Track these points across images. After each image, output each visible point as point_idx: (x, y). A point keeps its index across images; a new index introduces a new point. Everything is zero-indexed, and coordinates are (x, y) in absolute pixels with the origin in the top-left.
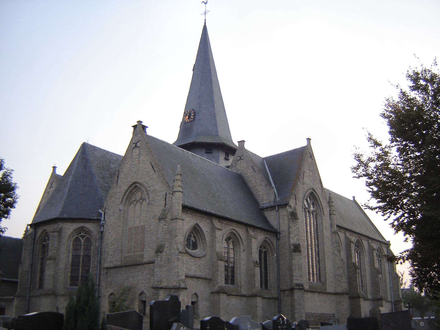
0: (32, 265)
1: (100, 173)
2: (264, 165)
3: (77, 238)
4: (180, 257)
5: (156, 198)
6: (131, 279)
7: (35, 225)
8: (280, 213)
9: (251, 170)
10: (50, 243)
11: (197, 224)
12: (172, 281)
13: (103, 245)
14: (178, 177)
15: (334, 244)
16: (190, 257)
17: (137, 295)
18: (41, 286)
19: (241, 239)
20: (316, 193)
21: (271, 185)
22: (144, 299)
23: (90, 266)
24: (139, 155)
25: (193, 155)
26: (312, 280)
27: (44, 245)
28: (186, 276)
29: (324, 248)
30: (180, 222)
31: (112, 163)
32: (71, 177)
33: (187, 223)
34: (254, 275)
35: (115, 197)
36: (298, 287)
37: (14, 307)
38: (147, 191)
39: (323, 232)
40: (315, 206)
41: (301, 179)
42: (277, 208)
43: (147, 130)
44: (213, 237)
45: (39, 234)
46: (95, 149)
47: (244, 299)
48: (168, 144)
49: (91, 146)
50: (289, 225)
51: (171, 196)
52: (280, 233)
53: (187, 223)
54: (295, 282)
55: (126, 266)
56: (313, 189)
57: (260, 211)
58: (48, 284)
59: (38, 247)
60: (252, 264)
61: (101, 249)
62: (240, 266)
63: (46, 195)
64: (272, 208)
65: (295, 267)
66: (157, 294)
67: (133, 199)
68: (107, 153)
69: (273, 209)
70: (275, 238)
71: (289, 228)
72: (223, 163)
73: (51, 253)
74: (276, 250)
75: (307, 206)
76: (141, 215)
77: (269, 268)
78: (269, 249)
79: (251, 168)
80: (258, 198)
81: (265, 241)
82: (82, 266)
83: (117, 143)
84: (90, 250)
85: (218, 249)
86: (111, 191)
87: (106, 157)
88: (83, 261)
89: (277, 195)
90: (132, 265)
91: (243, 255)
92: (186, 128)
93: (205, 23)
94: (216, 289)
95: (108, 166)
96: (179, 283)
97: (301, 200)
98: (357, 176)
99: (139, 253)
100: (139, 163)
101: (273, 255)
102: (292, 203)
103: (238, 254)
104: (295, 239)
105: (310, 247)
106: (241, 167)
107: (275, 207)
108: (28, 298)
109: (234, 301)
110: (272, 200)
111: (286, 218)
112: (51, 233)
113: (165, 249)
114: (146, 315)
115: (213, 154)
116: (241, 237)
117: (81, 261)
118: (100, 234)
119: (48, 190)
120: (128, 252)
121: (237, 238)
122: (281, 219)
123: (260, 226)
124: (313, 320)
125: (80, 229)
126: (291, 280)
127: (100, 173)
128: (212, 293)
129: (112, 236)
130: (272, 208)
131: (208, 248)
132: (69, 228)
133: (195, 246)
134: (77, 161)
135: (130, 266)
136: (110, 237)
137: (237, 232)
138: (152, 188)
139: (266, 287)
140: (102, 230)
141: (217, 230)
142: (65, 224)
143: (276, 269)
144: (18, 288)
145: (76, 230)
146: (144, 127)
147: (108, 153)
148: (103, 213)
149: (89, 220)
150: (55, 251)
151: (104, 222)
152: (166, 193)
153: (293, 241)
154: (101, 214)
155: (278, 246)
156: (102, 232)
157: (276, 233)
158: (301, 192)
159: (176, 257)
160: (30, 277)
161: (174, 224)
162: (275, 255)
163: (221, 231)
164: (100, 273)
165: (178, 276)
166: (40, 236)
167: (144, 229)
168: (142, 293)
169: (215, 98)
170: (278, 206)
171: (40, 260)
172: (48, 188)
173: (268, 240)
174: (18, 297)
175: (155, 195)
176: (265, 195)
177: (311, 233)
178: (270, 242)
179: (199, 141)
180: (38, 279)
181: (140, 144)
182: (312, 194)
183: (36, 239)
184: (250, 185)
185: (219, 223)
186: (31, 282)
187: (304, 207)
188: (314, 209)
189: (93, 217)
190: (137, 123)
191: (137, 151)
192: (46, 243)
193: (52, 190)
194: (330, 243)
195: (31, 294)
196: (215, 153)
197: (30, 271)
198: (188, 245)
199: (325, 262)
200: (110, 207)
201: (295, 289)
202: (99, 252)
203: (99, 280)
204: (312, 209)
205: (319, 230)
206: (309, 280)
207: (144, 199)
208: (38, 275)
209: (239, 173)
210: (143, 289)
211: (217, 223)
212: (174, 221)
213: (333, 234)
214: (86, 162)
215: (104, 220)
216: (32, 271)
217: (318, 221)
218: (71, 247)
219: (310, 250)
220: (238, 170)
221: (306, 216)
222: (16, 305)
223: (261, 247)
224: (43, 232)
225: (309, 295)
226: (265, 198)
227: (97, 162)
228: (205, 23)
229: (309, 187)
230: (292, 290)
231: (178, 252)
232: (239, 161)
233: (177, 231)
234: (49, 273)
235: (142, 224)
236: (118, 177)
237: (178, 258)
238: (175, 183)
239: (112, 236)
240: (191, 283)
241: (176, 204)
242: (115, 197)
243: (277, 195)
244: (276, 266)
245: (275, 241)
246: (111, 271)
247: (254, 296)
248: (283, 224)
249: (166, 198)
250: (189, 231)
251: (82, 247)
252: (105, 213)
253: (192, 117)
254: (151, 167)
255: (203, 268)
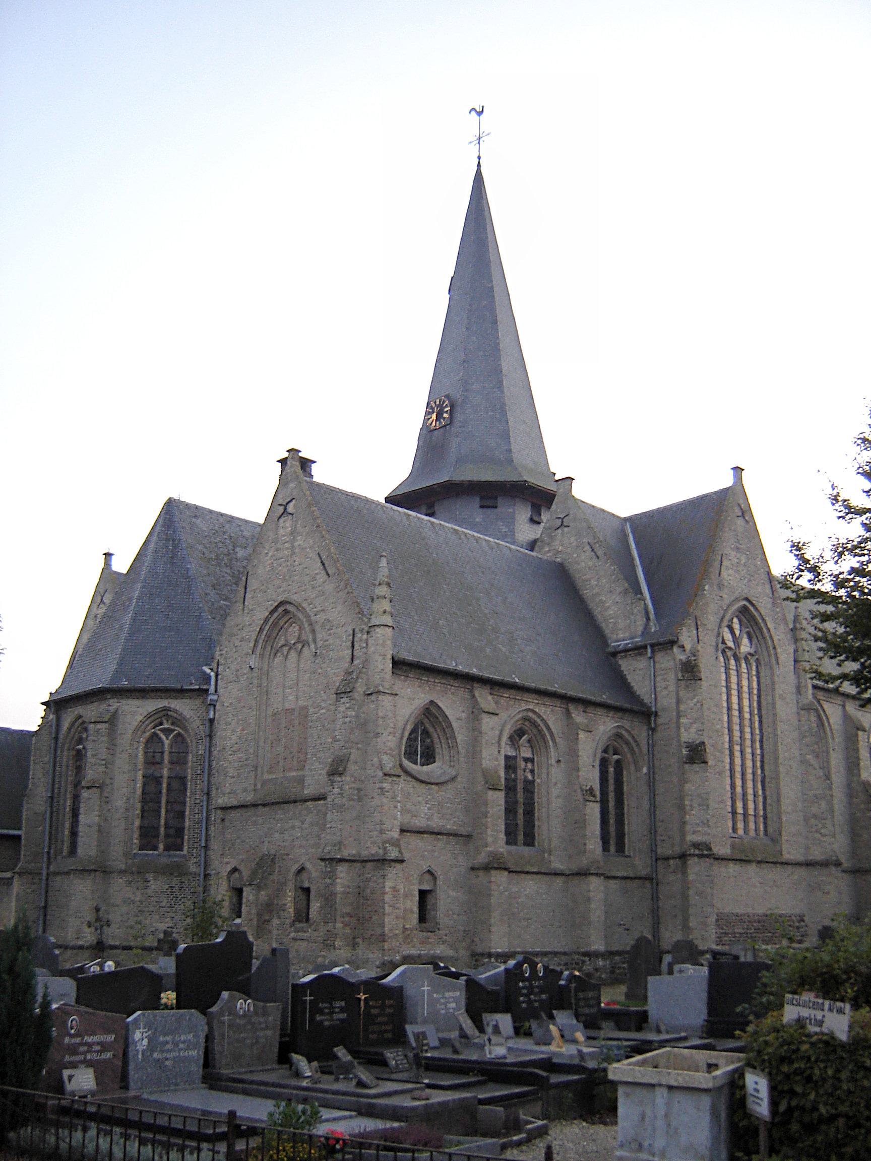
0: (52, 798)
1: (209, 574)
2: (625, 536)
3: (154, 734)
4: (385, 785)
5: (331, 641)
6: (277, 835)
7: (56, 705)
8: (657, 665)
9: (589, 553)
10: (90, 748)
11: (432, 702)
12: (369, 844)
13: (215, 753)
14: (383, 590)
15: (805, 737)
16: (414, 783)
17: (291, 875)
18: (73, 850)
19: (552, 735)
20: (756, 609)
21: (639, 591)
22: (306, 885)
23: (184, 803)
24: (292, 533)
25: (432, 523)
26: (741, 832)
27: (79, 751)
28: (402, 831)
29: (776, 751)
30: (386, 701)
31: (241, 546)
32: (139, 585)
33: (408, 700)
34: (581, 823)
35: (239, 637)
36: (697, 852)
37: (14, 900)
38: (311, 624)
39: (774, 707)
40: (755, 641)
41: (714, 576)
42: (649, 650)
43: (315, 469)
44: (476, 732)
45: (66, 725)
46: (197, 511)
47: (559, 881)
48: (367, 501)
49: (187, 506)
50: (677, 694)
51: (365, 636)
52: (656, 714)
53: (408, 700)
54: (690, 838)
55: (264, 805)
56: (747, 599)
57: (608, 659)
58: (87, 846)
59: (66, 756)
60: (580, 797)
61: (210, 761)
62: (549, 802)
63: (90, 622)
64: (639, 650)
65: (691, 800)
66: (332, 875)
67: (282, 642)
68: (229, 522)
69: (640, 654)
70: (645, 728)
71: (678, 701)
72: (526, 532)
73: (91, 774)
74: (646, 757)
75: (730, 644)
76: (299, 682)
77: (630, 803)
78: (629, 756)
79: (587, 548)
80: (603, 625)
81: (618, 736)
82: (167, 802)
83: (248, 497)
84: (185, 763)
85: (486, 763)
86: (231, 622)
87: (225, 532)
88: (168, 790)
89: (652, 616)
90: (278, 803)
91: (557, 774)
92: (431, 444)
93: (479, 165)
94: (482, 858)
95: (229, 554)
96: (385, 848)
97: (713, 630)
98: (794, 596)
99: (294, 774)
100: (293, 553)
101: (638, 770)
102: (686, 638)
103: (544, 771)
104: (693, 730)
105: (737, 748)
106: (565, 547)
107: (645, 647)
108: (44, 877)
109: (530, 886)
110: (640, 629)
111: (671, 676)
112: (92, 725)
113: (352, 767)
114: (311, 921)
115: (498, 510)
116: (549, 729)
117: (164, 791)
118: (208, 725)
119: (94, 611)
120: (271, 770)
121: (540, 731)
122: (658, 679)
123: (604, 698)
124: (742, 931)
125: (161, 714)
126: (683, 835)
127: (209, 574)
128: (473, 869)
129: (233, 731)
130: (639, 650)
131: (462, 759)
132: (134, 712)
133: (429, 757)
134: (152, 546)
135: (273, 804)
136: (229, 734)
137: (539, 716)
138: (321, 618)
139: (620, 848)
140: (211, 716)
141: (484, 715)
142: (124, 702)
143: (646, 806)
144: (22, 853)
145: (149, 716)
146: (306, 464)
147: (231, 519)
148: (212, 674)
149: (181, 692)
150: (102, 769)
151: (215, 697)
152: (354, 631)
153: (687, 736)
154: (208, 679)
155: (652, 747)
156: (212, 721)
157: (645, 714)
158: (712, 607)
159: (377, 785)
160: (47, 828)
161: (373, 706)
162: (645, 770)
163: (496, 718)
164: (208, 819)
165: (381, 832)
166: (69, 729)
167: (306, 717)
168: (302, 870)
169: (506, 365)
170: (652, 646)
171: (70, 788)
172: (95, 606)
173: (624, 732)
174: (20, 874)
175: (330, 635)
176: (622, 617)
177: (740, 710)
178: (630, 739)
179: (462, 478)
180: (67, 832)
181: (295, 506)
182: (744, 611)
183: (61, 737)
184: (587, 593)
185: (490, 697)
186: (50, 839)
187: (721, 646)
188: (752, 651)
189: (191, 683)
190: (287, 455)
191: (287, 524)
192: (84, 748)
193: (102, 610)
194: (796, 734)
195: (52, 868)
196: (505, 507)
197: (48, 813)
198: (410, 754)
199: (778, 784)
200: (229, 661)
201: (690, 855)
202: (207, 768)
203: (207, 835)
204: (745, 647)
205: (764, 703)
206: (735, 830)
207: (305, 644)
208: (67, 825)
209: (558, 560)
210: (303, 860)
211: (485, 699)
212: (373, 697)
213: (802, 712)
214: (175, 547)
215: (216, 691)
216: (52, 813)
217: (762, 680)
218: (141, 756)
219: (737, 754)
220: (557, 552)
221: (727, 669)
222: (18, 895)
223: (605, 751)
224: (76, 720)
225: (733, 868)
226: (622, 624)
227: (200, 547)
228: (479, 165)
229: (736, 594)
230: (683, 857)
231: (380, 774)
232: (559, 531)
233: (380, 722)
234: (88, 818)
235: (301, 703)
236: (246, 588)
237: (382, 788)
238: (375, 605)
239: (233, 731)
240: (414, 845)
241: (377, 657)
242: (239, 637)
243: (652, 616)
244: (647, 798)
245: (644, 734)
246: (233, 814)
247: (583, 873)
248: (665, 692)
249: (353, 642)
250: (412, 719)
251: (166, 757)
252: (217, 676)
253: (445, 415)
254: (319, 564)
255: (448, 808)
